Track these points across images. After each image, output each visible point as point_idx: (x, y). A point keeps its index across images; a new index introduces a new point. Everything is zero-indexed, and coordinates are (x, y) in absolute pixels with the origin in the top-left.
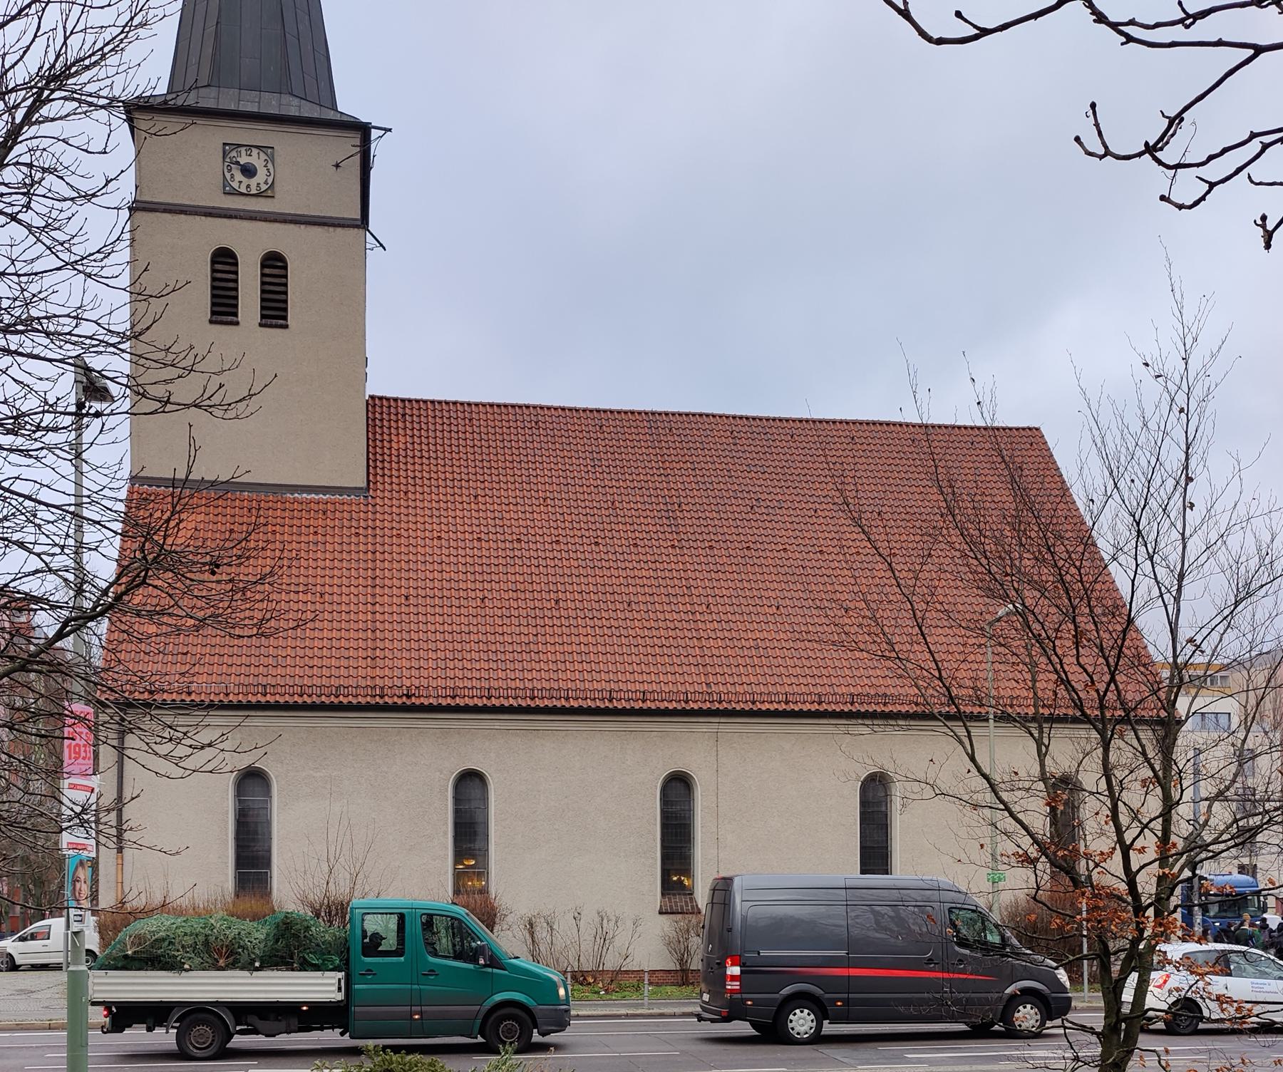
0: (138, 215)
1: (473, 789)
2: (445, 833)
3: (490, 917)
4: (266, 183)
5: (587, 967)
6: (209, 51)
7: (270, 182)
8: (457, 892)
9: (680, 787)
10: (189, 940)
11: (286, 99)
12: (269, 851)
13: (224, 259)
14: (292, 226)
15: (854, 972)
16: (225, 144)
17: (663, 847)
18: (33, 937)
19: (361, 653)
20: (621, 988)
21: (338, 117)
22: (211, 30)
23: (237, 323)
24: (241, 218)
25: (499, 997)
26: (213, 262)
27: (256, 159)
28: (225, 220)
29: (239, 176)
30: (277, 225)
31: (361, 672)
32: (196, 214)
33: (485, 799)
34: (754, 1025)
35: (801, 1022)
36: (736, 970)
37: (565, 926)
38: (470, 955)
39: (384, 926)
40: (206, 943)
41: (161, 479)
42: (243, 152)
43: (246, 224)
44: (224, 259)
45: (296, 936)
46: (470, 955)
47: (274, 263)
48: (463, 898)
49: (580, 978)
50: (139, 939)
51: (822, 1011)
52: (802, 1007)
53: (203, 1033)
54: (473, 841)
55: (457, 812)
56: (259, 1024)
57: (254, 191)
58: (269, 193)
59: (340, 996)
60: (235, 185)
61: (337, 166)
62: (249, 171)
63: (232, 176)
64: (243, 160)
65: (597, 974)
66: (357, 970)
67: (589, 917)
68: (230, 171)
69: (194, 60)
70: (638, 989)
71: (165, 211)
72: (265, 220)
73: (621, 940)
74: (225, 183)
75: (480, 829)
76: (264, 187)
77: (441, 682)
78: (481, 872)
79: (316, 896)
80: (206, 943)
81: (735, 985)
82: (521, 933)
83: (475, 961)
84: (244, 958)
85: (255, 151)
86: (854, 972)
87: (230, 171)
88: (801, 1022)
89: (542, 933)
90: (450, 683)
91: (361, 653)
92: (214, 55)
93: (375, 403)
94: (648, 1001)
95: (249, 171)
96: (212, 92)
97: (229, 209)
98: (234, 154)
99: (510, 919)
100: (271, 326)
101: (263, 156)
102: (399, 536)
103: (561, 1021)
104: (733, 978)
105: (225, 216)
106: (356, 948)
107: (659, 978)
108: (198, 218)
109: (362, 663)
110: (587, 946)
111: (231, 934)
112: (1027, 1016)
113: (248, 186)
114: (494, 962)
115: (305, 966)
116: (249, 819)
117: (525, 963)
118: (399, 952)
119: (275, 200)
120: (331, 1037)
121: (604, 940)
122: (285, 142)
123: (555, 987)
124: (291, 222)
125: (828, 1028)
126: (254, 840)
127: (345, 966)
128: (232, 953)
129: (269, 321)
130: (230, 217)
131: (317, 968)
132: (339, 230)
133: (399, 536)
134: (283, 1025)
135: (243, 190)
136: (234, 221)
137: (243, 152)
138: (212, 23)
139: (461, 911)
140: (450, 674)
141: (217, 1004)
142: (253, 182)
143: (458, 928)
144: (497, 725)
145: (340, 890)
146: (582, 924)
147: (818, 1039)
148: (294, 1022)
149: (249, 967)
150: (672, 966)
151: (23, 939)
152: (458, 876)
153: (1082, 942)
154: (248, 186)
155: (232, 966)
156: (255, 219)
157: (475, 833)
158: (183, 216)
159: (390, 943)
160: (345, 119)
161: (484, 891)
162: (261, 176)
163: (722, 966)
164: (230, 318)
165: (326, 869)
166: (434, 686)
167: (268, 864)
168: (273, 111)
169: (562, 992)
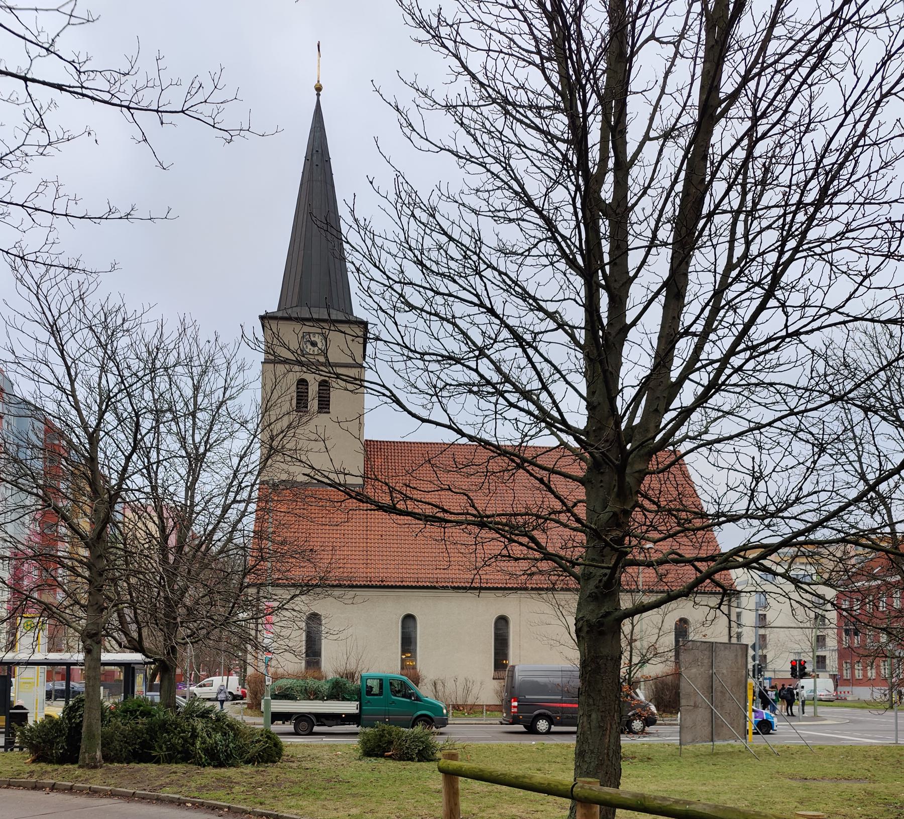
0: (266, 365)
1: (410, 623)
3: (417, 680)
5: (460, 703)
6: (297, 290)
8: (402, 668)
9: (503, 622)
10: (299, 688)
12: (320, 649)
13: (302, 382)
15: (564, 705)
17: (495, 649)
18: (204, 686)
19: (361, 562)
20: (475, 713)
21: (354, 319)
22: (298, 280)
25: (419, 713)
26: (298, 384)
29: (309, 346)
31: (361, 570)
33: (415, 627)
34: (525, 727)
35: (542, 725)
36: (515, 704)
37: (450, 685)
38: (409, 696)
39: (374, 684)
40: (306, 690)
44: (302, 382)
45: (340, 687)
46: (409, 696)
48: (405, 671)
49: (456, 707)
50: (280, 688)
51: (551, 721)
52: (543, 719)
53: (304, 725)
54: (410, 646)
55: (403, 633)
56: (326, 722)
59: (357, 711)
65: (464, 706)
66: (364, 701)
67: (461, 680)
69: (290, 294)
70: (482, 713)
73: (475, 690)
75: (413, 640)
77: (396, 575)
78: (414, 657)
79: (341, 669)
80: (306, 690)
81: (516, 710)
82: (431, 687)
83: (410, 698)
84: (320, 696)
86: (564, 705)
88: (542, 725)
89: (440, 687)
90: (400, 575)
91: (361, 562)
92: (299, 292)
93: (369, 444)
94: (484, 718)
96: (298, 309)
99: (425, 681)
103: (444, 723)
104: (515, 707)
106: (364, 692)
107: (491, 708)
109: (361, 566)
110: (460, 692)
111: (315, 686)
112: (637, 725)
114: (418, 699)
115: (344, 699)
117: (432, 699)
118: (381, 694)
120: (353, 728)
121: (468, 691)
123: (442, 709)
125: (554, 728)
127: (359, 699)
128: (315, 694)
131: (348, 700)
134: (335, 722)
138: (298, 277)
139: (405, 678)
140: (400, 571)
141: (310, 713)
143: (403, 684)
144: (421, 594)
145: (352, 667)
146: (458, 684)
147: (548, 732)
148: (339, 721)
149: (322, 699)
150: (498, 703)
151: (200, 686)
152: (403, 661)
155: (316, 699)
159: (376, 690)
161: (414, 668)
163: (510, 702)
165: (345, 657)
166: (393, 575)
167: (320, 655)
169: (445, 711)
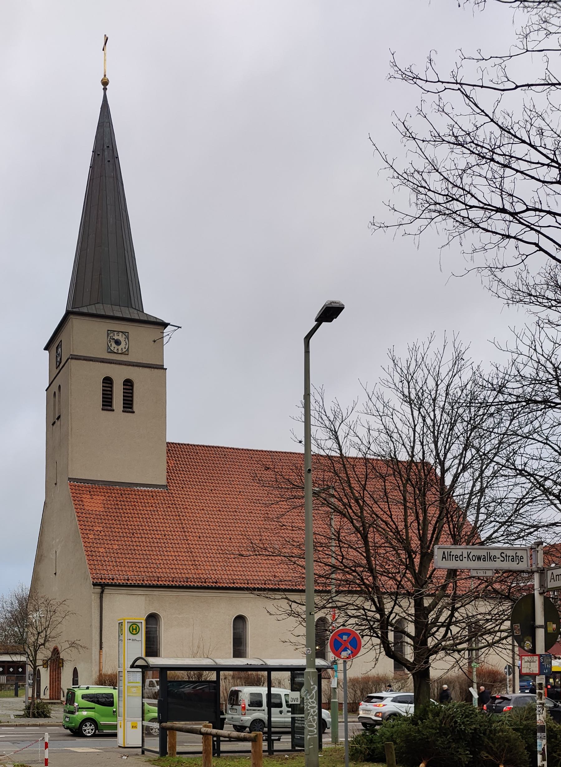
2: (230, 643)
4: (125, 348)
7: (127, 348)
11: (132, 310)
13: (108, 381)
14: (136, 368)
16: (108, 330)
23: (133, 412)
24: (116, 364)
27: (121, 337)
28: (109, 364)
29: (114, 345)
30: (130, 367)
32: (97, 361)
39: (61, 657)
41: (75, 479)
42: (116, 334)
43: (117, 366)
44: (108, 381)
47: (128, 384)
57: (120, 352)
58: (126, 353)
60: (112, 348)
61: (154, 341)
62: (118, 343)
63: (111, 345)
64: (116, 337)
68: (110, 342)
71: (84, 360)
72: (126, 365)
74: (109, 347)
76: (124, 350)
85: (121, 334)
87: (110, 342)
95: (118, 343)
96: (100, 306)
97: (109, 359)
98: (112, 335)
100: (128, 412)
101: (124, 336)
102: (187, 508)
105: (109, 363)
108: (97, 363)
113: (118, 349)
116: (150, 635)
119: (128, 356)
122: (133, 330)
124: (136, 366)
126: (153, 645)
129: (106, 407)
130: (111, 363)
132: (156, 370)
133: (187, 508)
135: (115, 351)
136: (112, 365)
137: (116, 334)
142: (120, 347)
153: (470, 692)
154: (118, 349)
156: (121, 364)
157: (241, 643)
158: (91, 362)
160: (158, 321)
162: (123, 345)
164: (109, 408)
168: (102, 313)
